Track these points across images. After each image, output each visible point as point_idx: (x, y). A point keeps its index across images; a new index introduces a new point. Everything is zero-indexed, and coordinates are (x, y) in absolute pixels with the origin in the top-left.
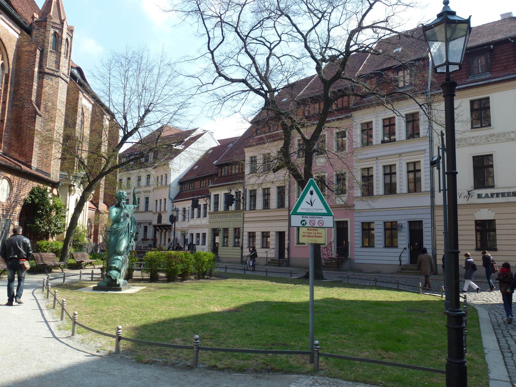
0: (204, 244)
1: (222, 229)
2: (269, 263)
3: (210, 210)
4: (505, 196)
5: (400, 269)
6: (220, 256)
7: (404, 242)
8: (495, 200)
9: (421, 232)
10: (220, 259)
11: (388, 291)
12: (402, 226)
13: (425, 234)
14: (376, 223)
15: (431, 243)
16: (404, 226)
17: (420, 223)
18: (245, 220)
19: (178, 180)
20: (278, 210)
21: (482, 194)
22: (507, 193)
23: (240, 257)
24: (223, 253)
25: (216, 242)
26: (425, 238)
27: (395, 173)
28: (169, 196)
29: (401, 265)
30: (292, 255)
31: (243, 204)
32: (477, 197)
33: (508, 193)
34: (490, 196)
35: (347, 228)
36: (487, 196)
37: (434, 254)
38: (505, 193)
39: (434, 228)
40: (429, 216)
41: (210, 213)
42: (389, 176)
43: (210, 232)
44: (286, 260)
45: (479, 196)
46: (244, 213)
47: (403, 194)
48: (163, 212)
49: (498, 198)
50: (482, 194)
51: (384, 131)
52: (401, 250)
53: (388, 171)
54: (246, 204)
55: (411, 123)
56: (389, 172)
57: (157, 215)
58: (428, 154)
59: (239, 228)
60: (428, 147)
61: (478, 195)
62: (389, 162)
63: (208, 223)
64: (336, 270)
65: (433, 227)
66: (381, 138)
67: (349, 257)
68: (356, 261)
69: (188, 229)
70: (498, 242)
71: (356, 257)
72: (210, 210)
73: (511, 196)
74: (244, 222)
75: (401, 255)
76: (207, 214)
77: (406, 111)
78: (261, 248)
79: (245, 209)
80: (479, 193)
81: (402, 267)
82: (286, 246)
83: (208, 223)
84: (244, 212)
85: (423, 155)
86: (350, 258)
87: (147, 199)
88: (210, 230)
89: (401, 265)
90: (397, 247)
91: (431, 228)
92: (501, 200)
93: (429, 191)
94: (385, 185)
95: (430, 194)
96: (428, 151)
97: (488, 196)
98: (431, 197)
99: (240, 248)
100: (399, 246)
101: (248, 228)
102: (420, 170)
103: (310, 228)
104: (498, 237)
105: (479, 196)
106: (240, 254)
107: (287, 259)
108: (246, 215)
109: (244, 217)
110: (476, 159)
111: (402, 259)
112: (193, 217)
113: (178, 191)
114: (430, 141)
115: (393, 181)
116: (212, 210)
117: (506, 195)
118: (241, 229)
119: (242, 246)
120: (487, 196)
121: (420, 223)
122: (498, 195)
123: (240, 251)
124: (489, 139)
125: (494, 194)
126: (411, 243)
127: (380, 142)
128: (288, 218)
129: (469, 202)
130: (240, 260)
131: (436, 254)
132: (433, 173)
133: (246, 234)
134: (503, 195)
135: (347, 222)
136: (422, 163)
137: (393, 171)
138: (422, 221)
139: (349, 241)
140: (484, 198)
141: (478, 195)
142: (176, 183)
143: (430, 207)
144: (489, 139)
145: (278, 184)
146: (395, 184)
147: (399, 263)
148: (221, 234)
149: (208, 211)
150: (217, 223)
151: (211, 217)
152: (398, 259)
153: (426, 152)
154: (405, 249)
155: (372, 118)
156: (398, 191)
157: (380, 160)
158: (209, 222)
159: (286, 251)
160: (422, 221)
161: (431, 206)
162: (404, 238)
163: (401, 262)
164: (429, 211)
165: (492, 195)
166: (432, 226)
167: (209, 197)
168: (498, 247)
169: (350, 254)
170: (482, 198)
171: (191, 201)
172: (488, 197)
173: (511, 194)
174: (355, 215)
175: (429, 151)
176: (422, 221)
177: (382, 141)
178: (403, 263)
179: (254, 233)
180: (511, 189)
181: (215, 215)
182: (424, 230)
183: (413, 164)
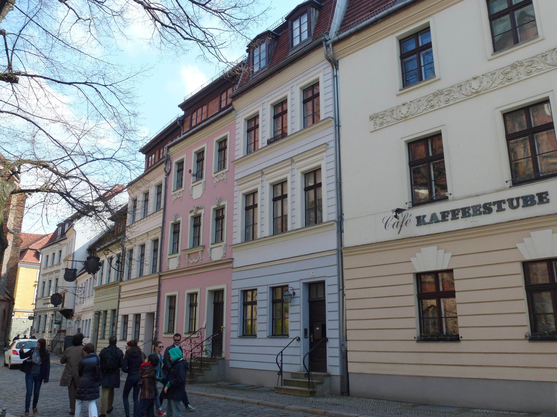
4: (469, 216)
8: (450, 225)
12: (294, 294)
14: (259, 289)
15: (337, 327)
19: (87, 247)
21: (424, 216)
22: (473, 207)
24: (240, 357)
29: (281, 372)
32: (416, 223)
33: (474, 207)
34: (440, 217)
35: (222, 303)
36: (434, 219)
37: (343, 349)
38: (469, 208)
39: (344, 295)
40: (334, 271)
45: (420, 221)
46: (120, 286)
49: (455, 221)
50: (424, 216)
54: (123, 272)
58: (332, 151)
59: (153, 314)
60: (332, 137)
61: (418, 218)
65: (341, 292)
68: (232, 364)
69: (81, 313)
70: (461, 321)
71: (232, 357)
73: (480, 214)
74: (121, 300)
75: (282, 352)
80: (418, 215)
81: (285, 377)
84: (121, 284)
85: (325, 154)
86: (224, 359)
87: (217, 295)
89: (281, 372)
90: (288, 335)
92: (461, 223)
96: (332, 144)
97: (437, 218)
104: (460, 310)
105: (420, 221)
108: (123, 289)
109: (120, 291)
110: (421, 149)
114: (336, 125)
117: (471, 212)
120: (434, 219)
122: (454, 214)
124: (433, 103)
125: (448, 212)
127: (266, 144)
128: (157, 290)
129: (400, 236)
131: (347, 351)
134: (465, 212)
138: (323, 283)
140: (429, 223)
141: (418, 218)
142: (84, 251)
143: (335, 252)
144: (433, 103)
145: (153, 237)
153: (330, 146)
154: (299, 339)
157: (267, 174)
158: (95, 303)
164: (334, 260)
165: (444, 215)
166: (339, 290)
168: (462, 333)
169: (224, 350)
170: (425, 224)
172: (438, 221)
173: (482, 210)
174: (235, 276)
177: (268, 141)
178: (285, 368)
180: (481, 197)
182: (328, 299)
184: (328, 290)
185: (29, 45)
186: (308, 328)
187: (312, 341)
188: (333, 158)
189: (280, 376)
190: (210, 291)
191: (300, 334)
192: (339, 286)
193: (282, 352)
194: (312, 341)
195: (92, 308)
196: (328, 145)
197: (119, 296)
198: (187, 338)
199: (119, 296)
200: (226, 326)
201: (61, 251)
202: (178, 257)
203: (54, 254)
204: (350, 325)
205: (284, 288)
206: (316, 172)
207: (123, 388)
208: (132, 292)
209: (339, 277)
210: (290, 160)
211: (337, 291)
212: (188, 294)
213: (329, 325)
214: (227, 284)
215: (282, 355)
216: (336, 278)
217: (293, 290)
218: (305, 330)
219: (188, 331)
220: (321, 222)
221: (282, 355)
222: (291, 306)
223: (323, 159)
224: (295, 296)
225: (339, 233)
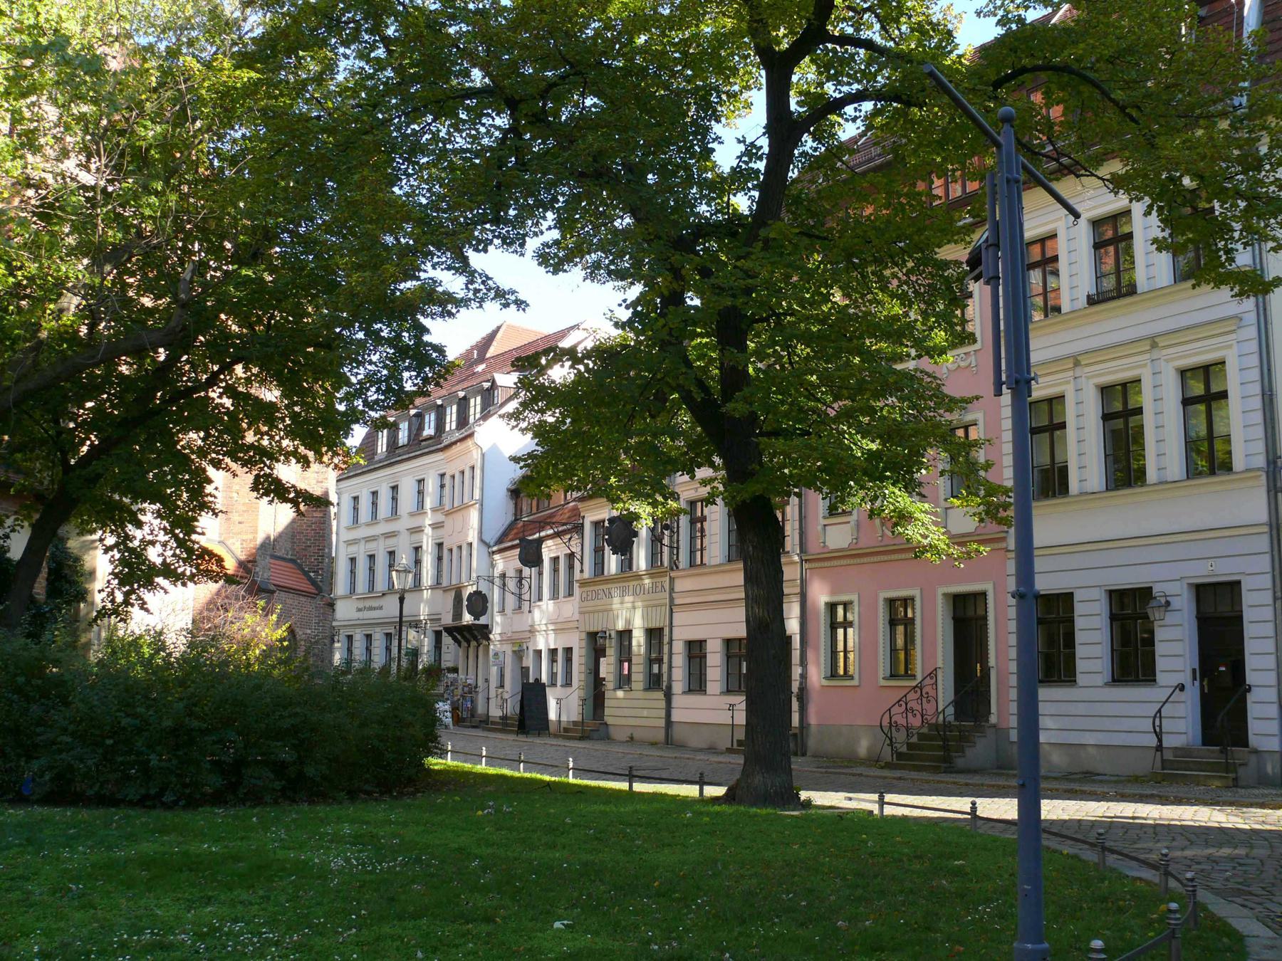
0: (568, 683)
1: (613, 634)
2: (900, 756)
3: (582, 571)
5: (1158, 764)
6: (609, 720)
7: (1178, 664)
9: (1236, 621)
10: (612, 730)
11: (689, 786)
12: (1168, 603)
13: (1249, 630)
16: (1176, 603)
17: (1233, 588)
18: (677, 601)
20: (727, 567)
23: (662, 723)
24: (619, 712)
25: (602, 675)
26: (1250, 647)
27: (1224, 395)
28: (481, 532)
29: (1160, 748)
30: (813, 719)
31: (671, 547)
35: (985, 618)
41: (583, 583)
42: (1047, 434)
43: (584, 644)
44: (795, 735)
46: (672, 580)
47: (1167, 482)
48: (410, 591)
51: (1098, 261)
52: (1161, 694)
53: (1198, 389)
54: (678, 548)
55: (1111, 249)
56: (1202, 392)
57: (453, 593)
58: (1252, 332)
59: (661, 630)
62: (1115, 373)
63: (577, 616)
64: (936, 770)
66: (1086, 285)
67: (993, 719)
72: (582, 571)
75: (1160, 711)
76: (576, 585)
77: (1094, 208)
78: (722, 693)
79: (674, 565)
81: (1169, 756)
82: (795, 687)
83: (577, 616)
84: (673, 574)
85: (1234, 336)
86: (994, 726)
88: (584, 636)
89: (1160, 748)
91: (1271, 608)
93: (1258, 469)
94: (1191, 445)
95: (1264, 477)
98: (1269, 492)
99: (660, 695)
100: (1160, 677)
101: (685, 628)
102: (1139, 411)
103: (395, 643)
106: (663, 713)
107: (797, 731)
108: (680, 585)
109: (672, 590)
111: (1167, 725)
112: (540, 600)
113: (510, 518)
115: (1219, 429)
116: (587, 574)
118: (666, 631)
119: (669, 687)
121: (1233, 588)
123: (663, 704)
126: (1206, 669)
127: (1083, 302)
130: (661, 736)
132: (1271, 401)
133: (679, 647)
135: (983, 594)
136: (1232, 370)
137: (1215, 388)
138: (1072, 594)
139: (992, 661)
143: (1266, 529)
146: (1227, 439)
147: (1152, 741)
148: (611, 652)
149: (577, 575)
150: (592, 615)
151: (584, 595)
152: (1147, 725)
154: (1182, 687)
155: (1056, 220)
156: (1152, 475)
157: (1087, 365)
158: (580, 613)
159: (795, 705)
160: (1072, 594)
161: (1271, 526)
162: (1178, 648)
163: (1160, 740)
167: (579, 529)
169: (994, 709)
171: (517, 551)
175: (1254, 320)
176: (1239, 583)
177: (1088, 296)
178: (1168, 742)
179: (701, 643)
181: (596, 588)
182: (1248, 615)
183: (1045, 407)
184: (1248, 598)
185: (998, 73)
186: (1197, 667)
187: (1206, 691)
188: (1254, 346)
189: (1159, 753)
190: (945, 595)
191: (1185, 678)
192: (1275, 593)
193: (1160, 711)
194: (1206, 691)
195: (575, 624)
196: (1241, 319)
197: (672, 599)
198: (915, 687)
199: (672, 599)
200: (997, 663)
201: (395, 488)
202: (852, 523)
203: (375, 494)
204: (596, 615)
205: (1145, 594)
206: (1208, 371)
207: (1068, 802)
208: (728, 590)
209: (1274, 577)
210: (1149, 342)
211: (1270, 601)
212: (886, 600)
213: (1251, 662)
214: (994, 584)
215: (1161, 717)
216: (1269, 577)
217: (1166, 596)
218: (1194, 671)
219: (888, 674)
220: (1227, 467)
221: (1161, 717)
222: (1160, 626)
223: (1230, 346)
224: (1169, 608)
225: (1272, 493)
